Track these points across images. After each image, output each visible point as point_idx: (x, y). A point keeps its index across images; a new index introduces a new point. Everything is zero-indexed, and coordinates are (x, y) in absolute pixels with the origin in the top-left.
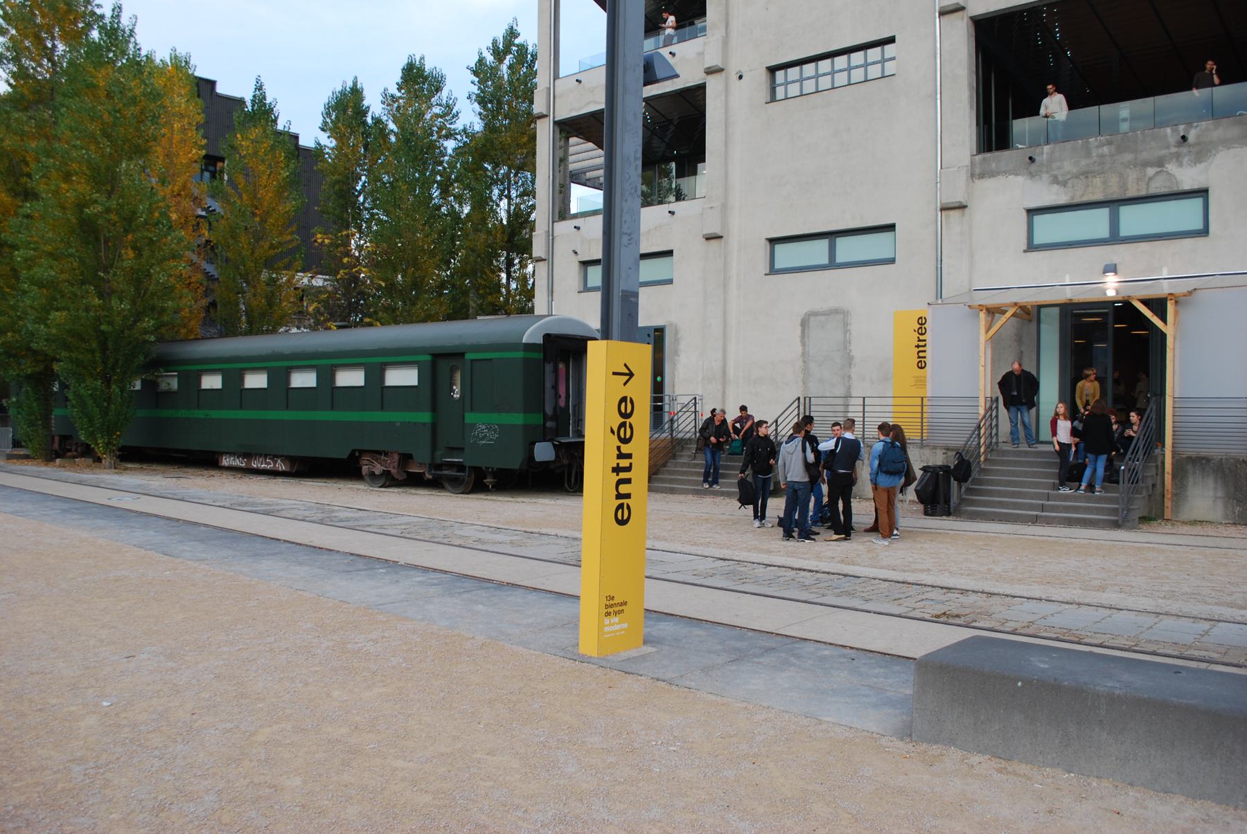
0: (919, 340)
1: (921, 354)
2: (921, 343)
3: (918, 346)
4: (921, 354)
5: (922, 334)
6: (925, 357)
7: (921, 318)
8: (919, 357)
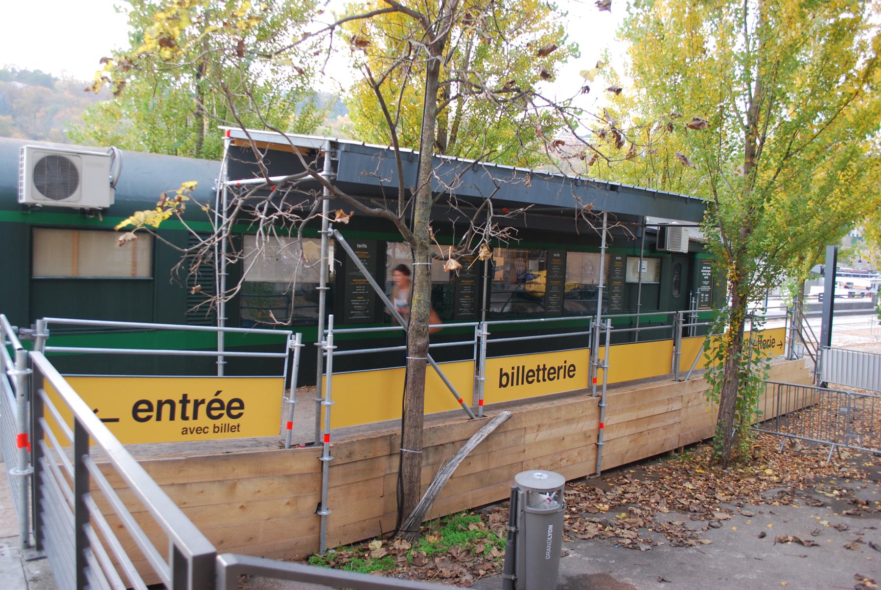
0: (197, 404)
1: (166, 408)
2: (190, 407)
3: (185, 401)
4: (166, 408)
5: (209, 409)
6: (159, 418)
7: (242, 407)
8: (160, 404)
